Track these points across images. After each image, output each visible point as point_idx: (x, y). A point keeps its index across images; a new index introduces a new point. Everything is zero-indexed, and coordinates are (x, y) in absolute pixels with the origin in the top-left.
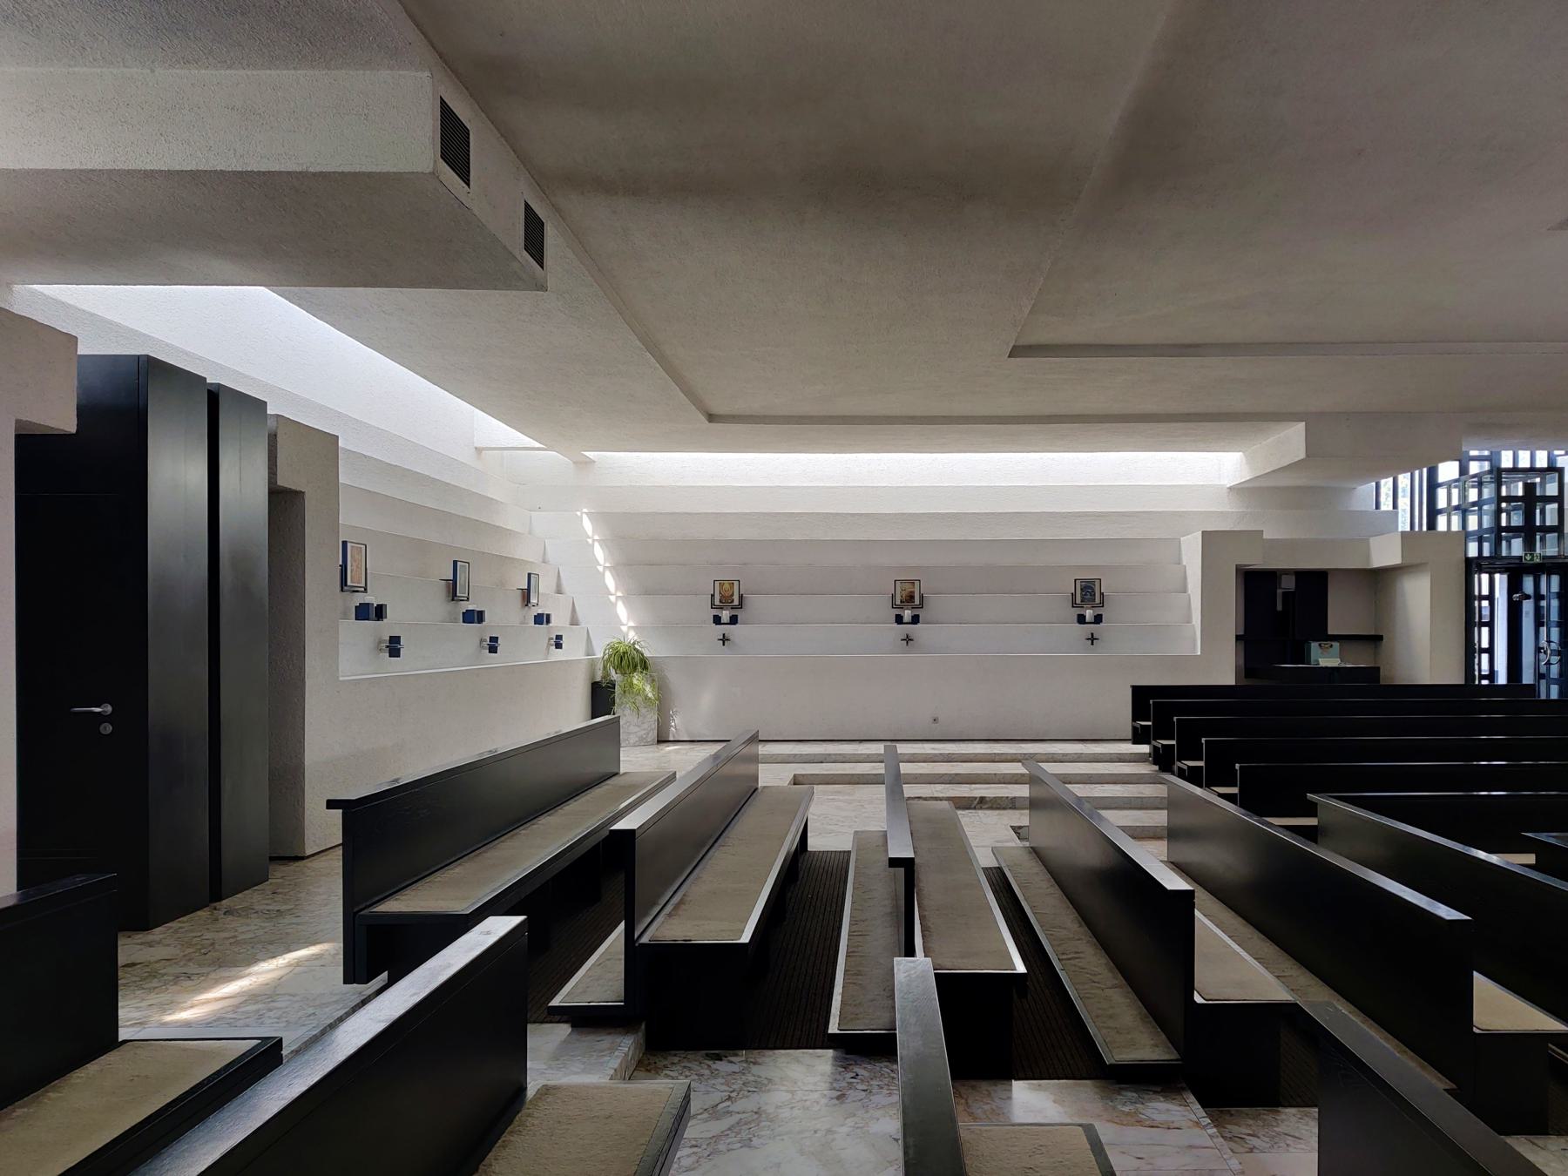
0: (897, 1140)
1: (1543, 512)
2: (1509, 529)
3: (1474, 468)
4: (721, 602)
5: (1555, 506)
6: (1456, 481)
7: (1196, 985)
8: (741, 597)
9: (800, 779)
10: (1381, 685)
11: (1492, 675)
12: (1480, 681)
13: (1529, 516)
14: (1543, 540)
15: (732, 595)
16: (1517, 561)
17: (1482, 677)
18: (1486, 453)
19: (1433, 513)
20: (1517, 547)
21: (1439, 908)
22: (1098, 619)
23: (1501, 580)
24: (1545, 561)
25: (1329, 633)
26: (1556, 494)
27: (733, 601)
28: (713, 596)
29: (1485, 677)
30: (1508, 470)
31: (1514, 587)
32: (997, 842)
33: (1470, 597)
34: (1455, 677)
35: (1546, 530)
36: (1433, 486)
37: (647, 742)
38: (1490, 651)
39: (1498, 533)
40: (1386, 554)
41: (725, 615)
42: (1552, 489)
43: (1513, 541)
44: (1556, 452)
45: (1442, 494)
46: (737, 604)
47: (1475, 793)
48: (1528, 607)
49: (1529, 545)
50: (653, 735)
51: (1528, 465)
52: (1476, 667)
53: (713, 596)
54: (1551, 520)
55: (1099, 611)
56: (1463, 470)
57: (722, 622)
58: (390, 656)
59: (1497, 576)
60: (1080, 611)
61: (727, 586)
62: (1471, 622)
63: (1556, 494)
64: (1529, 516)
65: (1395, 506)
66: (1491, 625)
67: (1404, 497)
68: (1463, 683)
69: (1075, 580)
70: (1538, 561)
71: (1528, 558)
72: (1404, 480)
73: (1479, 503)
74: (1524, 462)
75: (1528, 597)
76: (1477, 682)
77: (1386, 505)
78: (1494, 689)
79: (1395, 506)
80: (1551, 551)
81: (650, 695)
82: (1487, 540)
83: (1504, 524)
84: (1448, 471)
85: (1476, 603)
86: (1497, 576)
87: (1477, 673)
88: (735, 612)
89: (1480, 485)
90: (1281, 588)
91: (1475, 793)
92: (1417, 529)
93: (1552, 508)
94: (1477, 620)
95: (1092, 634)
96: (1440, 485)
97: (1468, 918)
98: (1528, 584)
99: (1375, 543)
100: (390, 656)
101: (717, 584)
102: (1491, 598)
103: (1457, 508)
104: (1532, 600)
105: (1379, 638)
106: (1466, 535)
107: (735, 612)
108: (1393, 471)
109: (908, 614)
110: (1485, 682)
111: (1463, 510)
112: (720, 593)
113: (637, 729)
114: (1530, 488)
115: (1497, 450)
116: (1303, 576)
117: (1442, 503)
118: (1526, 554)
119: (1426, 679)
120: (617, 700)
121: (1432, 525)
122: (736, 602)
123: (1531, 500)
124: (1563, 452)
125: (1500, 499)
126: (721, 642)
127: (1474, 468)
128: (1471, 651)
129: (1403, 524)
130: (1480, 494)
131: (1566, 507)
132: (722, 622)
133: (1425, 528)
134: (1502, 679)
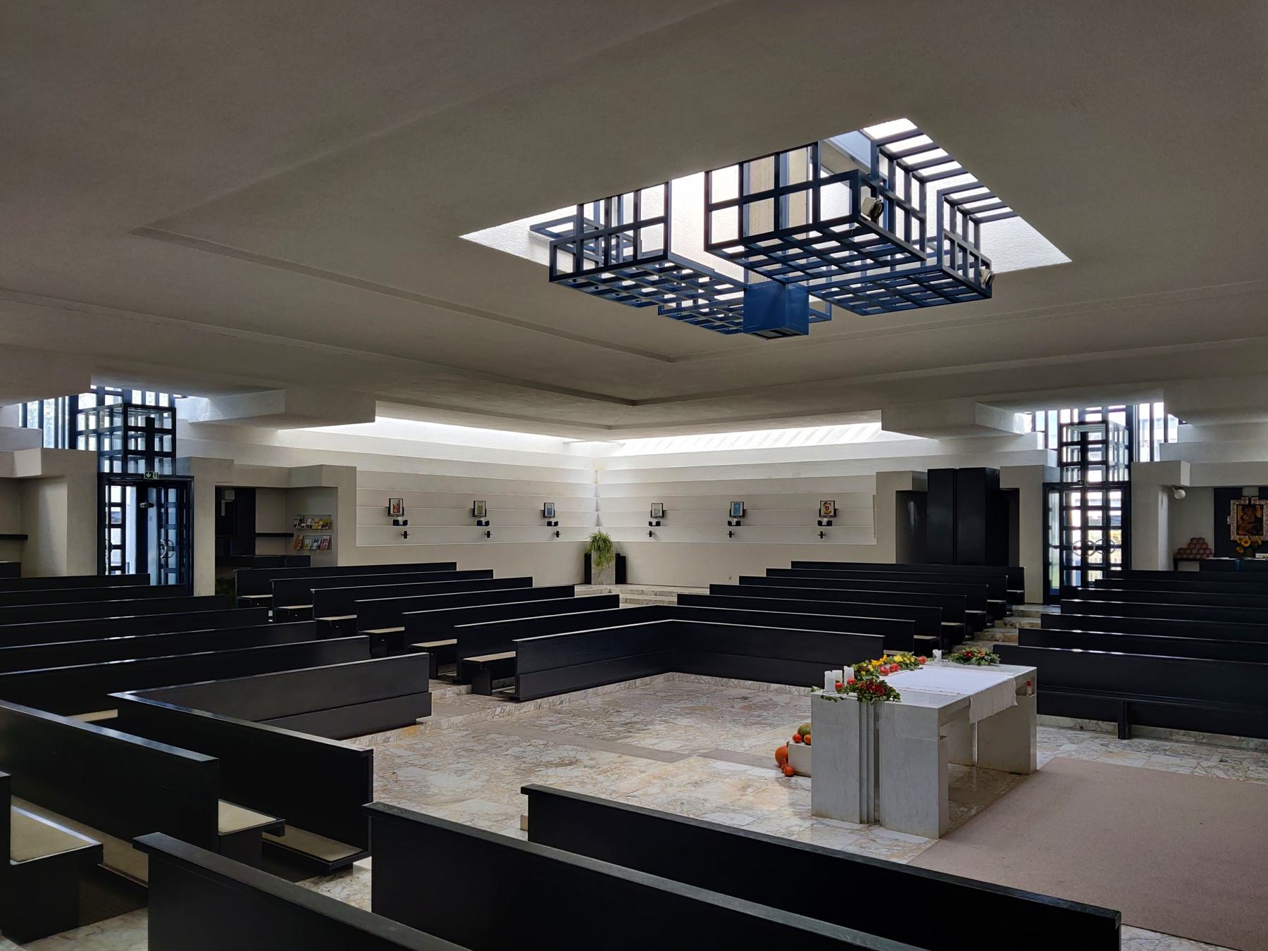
0: (1180, 943)
1: (161, 440)
2: (136, 452)
3: (109, 400)
5: (170, 436)
6: (94, 409)
7: (12, 855)
10: (23, 579)
11: (123, 567)
12: (110, 573)
13: (150, 444)
14: (161, 461)
16: (140, 478)
17: (113, 569)
18: (120, 390)
19: (74, 434)
20: (142, 467)
21: (173, 750)
23: (131, 492)
24: (162, 479)
25: (257, 532)
26: (170, 428)
29: (116, 568)
30: (136, 406)
31: (141, 497)
33: (102, 504)
34: (90, 570)
35: (162, 454)
36: (74, 411)
38: (122, 547)
39: (126, 454)
40: (29, 465)
41: (825, 520)
42: (168, 425)
43: (139, 461)
44: (175, 396)
45: (81, 418)
47: (106, 663)
48: (152, 512)
49: (150, 465)
51: (153, 404)
52: (107, 561)
54: (167, 448)
56: (101, 402)
58: (356, 468)
59: (128, 489)
62: (102, 523)
63: (170, 428)
64: (150, 444)
65: (41, 425)
66: (122, 526)
67: (49, 419)
68: (96, 574)
70: (156, 478)
71: (148, 475)
72: (49, 405)
73: (112, 430)
74: (150, 401)
75: (152, 506)
76: (107, 573)
77: (33, 423)
78: (125, 578)
79: (41, 425)
80: (167, 470)
82: (117, 459)
83: (157, 448)
84: (87, 401)
85: (107, 509)
86: (128, 489)
87: (107, 566)
89: (112, 416)
90: (225, 500)
91: (106, 663)
92: (60, 447)
93: (167, 438)
94: (107, 523)
95: (822, 537)
96: (81, 411)
97: (212, 758)
98: (153, 494)
99: (19, 456)
100: (356, 468)
102: (122, 505)
103: (95, 431)
104: (155, 508)
105: (24, 538)
106: (100, 453)
107: (830, 519)
108: (41, 396)
110: (118, 573)
111: (99, 434)
114: (150, 421)
115: (129, 389)
116: (239, 491)
117: (81, 426)
118: (147, 473)
119: (64, 573)
121: (73, 444)
122: (741, 514)
123: (150, 431)
124: (180, 396)
125: (126, 428)
127: (109, 400)
128: (102, 547)
129: (49, 443)
130: (112, 422)
131: (177, 437)
133: (67, 448)
134: (132, 570)
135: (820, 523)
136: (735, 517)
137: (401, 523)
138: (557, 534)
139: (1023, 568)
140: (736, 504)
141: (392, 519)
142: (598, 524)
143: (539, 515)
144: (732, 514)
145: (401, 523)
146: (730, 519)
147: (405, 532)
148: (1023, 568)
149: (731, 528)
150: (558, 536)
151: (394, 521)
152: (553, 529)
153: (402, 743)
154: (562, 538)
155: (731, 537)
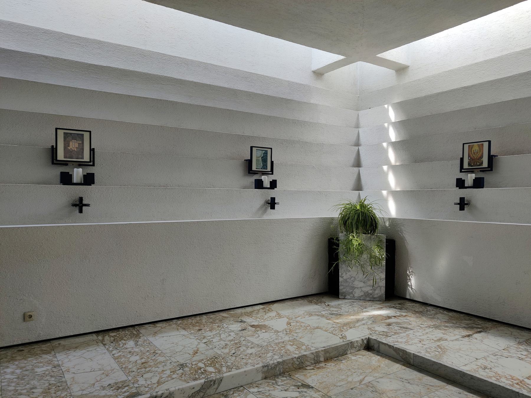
4: (469, 164)
8: (491, 158)
9: (372, 343)
15: (482, 157)
22: (273, 184)
27: (482, 163)
28: (462, 160)
32: (23, 350)
37: (375, 298)
41: (470, 178)
46: (487, 166)
50: (381, 291)
53: (462, 160)
55: (90, 170)
57: (466, 185)
60: (256, 177)
61: (476, 148)
69: (252, 147)
81: (377, 254)
88: (481, 175)
95: (81, 199)
101: (466, 146)
107: (481, 175)
109: (471, 177)
112: (469, 156)
113: (362, 284)
120: (341, 256)
122: (485, 164)
126: (84, 202)
132: (466, 185)
135: (460, 183)
136: (471, 171)
137: (267, 184)
138: (272, 203)
139: (274, 189)
140: (471, 144)
141: (57, 171)
142: (358, 187)
143: (239, 171)
144: (466, 166)
145: (267, 184)
146: (462, 176)
147: (273, 199)
148: (274, 189)
149: (463, 193)
150: (273, 207)
151: (62, 174)
152: (262, 196)
153: (325, 383)
154: (272, 215)
155: (462, 208)
